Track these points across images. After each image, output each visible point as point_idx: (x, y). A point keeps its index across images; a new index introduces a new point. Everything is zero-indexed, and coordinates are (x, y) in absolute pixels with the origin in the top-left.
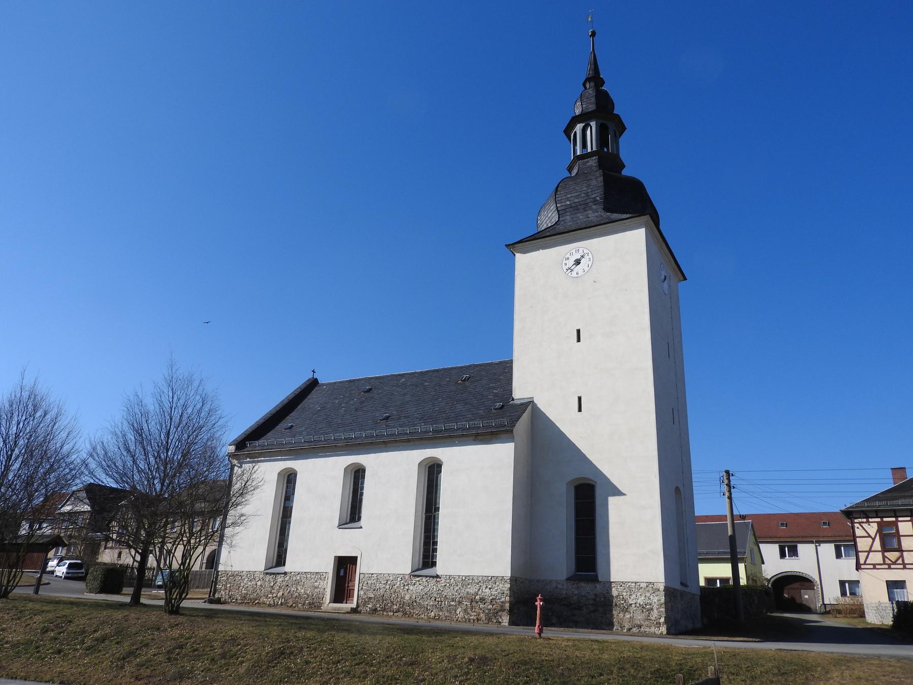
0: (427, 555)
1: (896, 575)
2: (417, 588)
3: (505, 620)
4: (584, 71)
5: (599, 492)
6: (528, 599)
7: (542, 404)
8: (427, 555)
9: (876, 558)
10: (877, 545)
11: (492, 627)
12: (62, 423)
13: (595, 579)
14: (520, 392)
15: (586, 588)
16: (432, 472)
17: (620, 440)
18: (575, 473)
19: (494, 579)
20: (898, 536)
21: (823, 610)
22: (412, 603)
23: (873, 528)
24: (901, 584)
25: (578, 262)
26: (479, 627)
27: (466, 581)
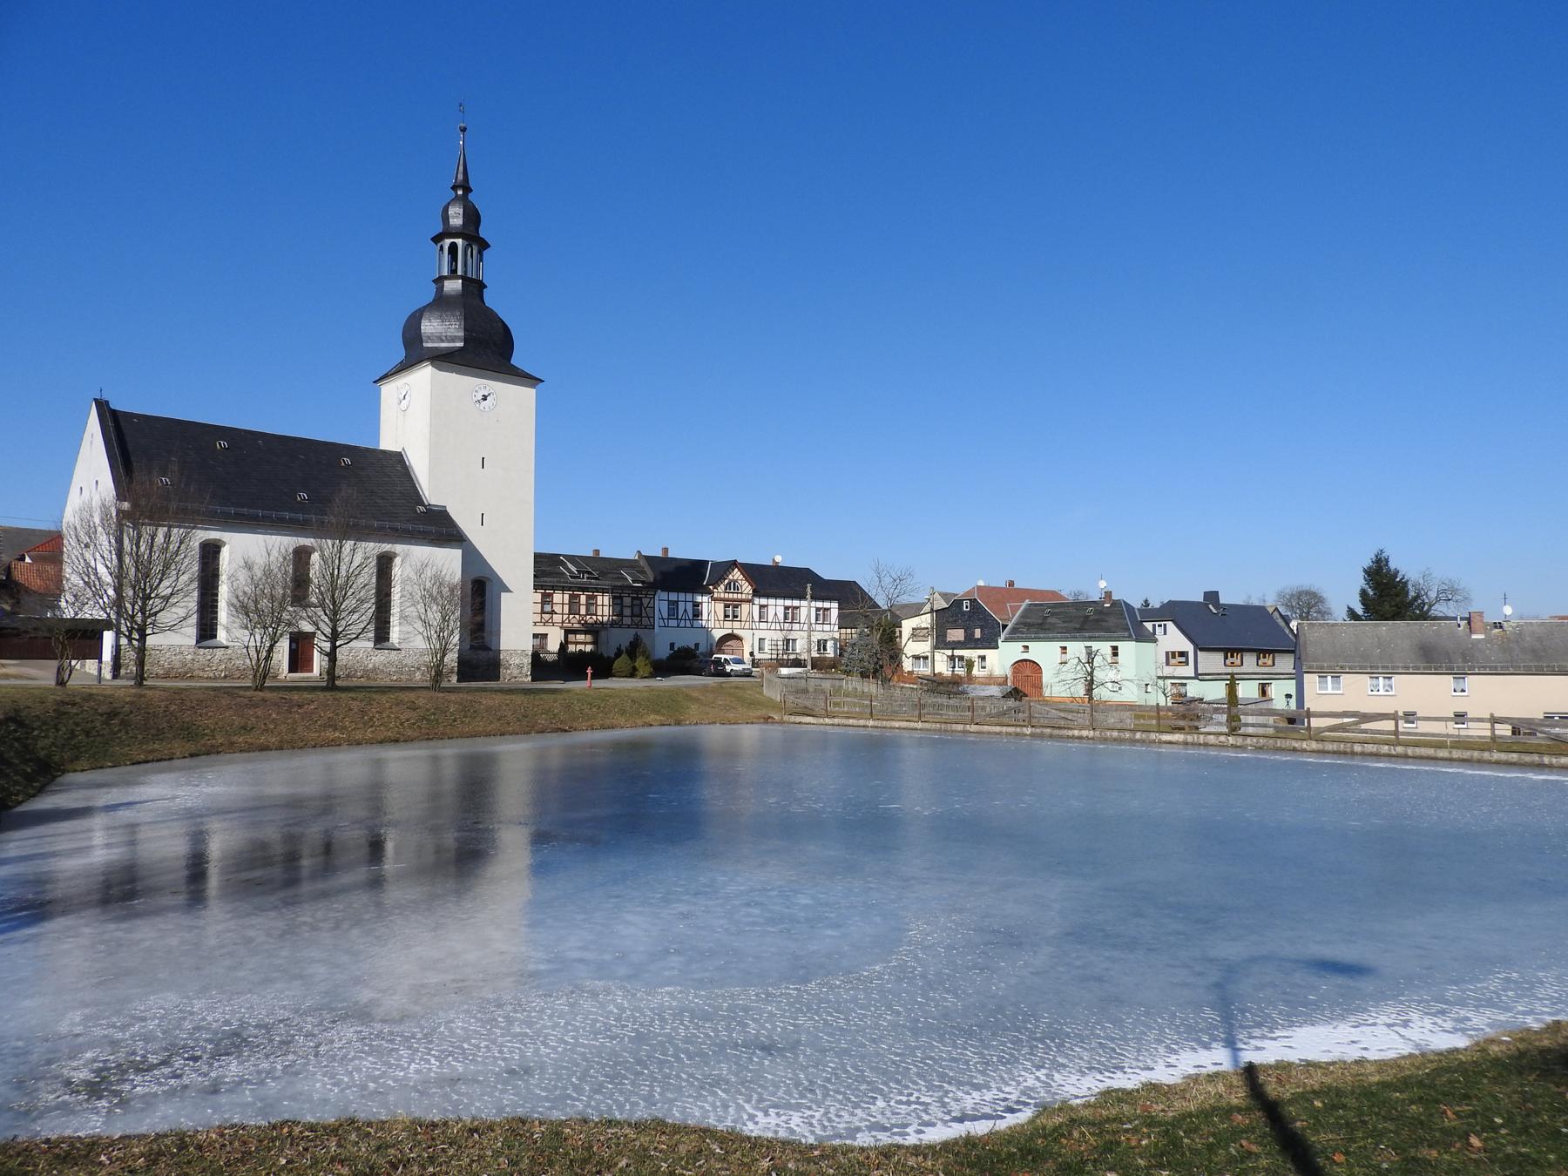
3: (454, 679)
4: (452, 176)
15: (483, 655)
22: (375, 669)
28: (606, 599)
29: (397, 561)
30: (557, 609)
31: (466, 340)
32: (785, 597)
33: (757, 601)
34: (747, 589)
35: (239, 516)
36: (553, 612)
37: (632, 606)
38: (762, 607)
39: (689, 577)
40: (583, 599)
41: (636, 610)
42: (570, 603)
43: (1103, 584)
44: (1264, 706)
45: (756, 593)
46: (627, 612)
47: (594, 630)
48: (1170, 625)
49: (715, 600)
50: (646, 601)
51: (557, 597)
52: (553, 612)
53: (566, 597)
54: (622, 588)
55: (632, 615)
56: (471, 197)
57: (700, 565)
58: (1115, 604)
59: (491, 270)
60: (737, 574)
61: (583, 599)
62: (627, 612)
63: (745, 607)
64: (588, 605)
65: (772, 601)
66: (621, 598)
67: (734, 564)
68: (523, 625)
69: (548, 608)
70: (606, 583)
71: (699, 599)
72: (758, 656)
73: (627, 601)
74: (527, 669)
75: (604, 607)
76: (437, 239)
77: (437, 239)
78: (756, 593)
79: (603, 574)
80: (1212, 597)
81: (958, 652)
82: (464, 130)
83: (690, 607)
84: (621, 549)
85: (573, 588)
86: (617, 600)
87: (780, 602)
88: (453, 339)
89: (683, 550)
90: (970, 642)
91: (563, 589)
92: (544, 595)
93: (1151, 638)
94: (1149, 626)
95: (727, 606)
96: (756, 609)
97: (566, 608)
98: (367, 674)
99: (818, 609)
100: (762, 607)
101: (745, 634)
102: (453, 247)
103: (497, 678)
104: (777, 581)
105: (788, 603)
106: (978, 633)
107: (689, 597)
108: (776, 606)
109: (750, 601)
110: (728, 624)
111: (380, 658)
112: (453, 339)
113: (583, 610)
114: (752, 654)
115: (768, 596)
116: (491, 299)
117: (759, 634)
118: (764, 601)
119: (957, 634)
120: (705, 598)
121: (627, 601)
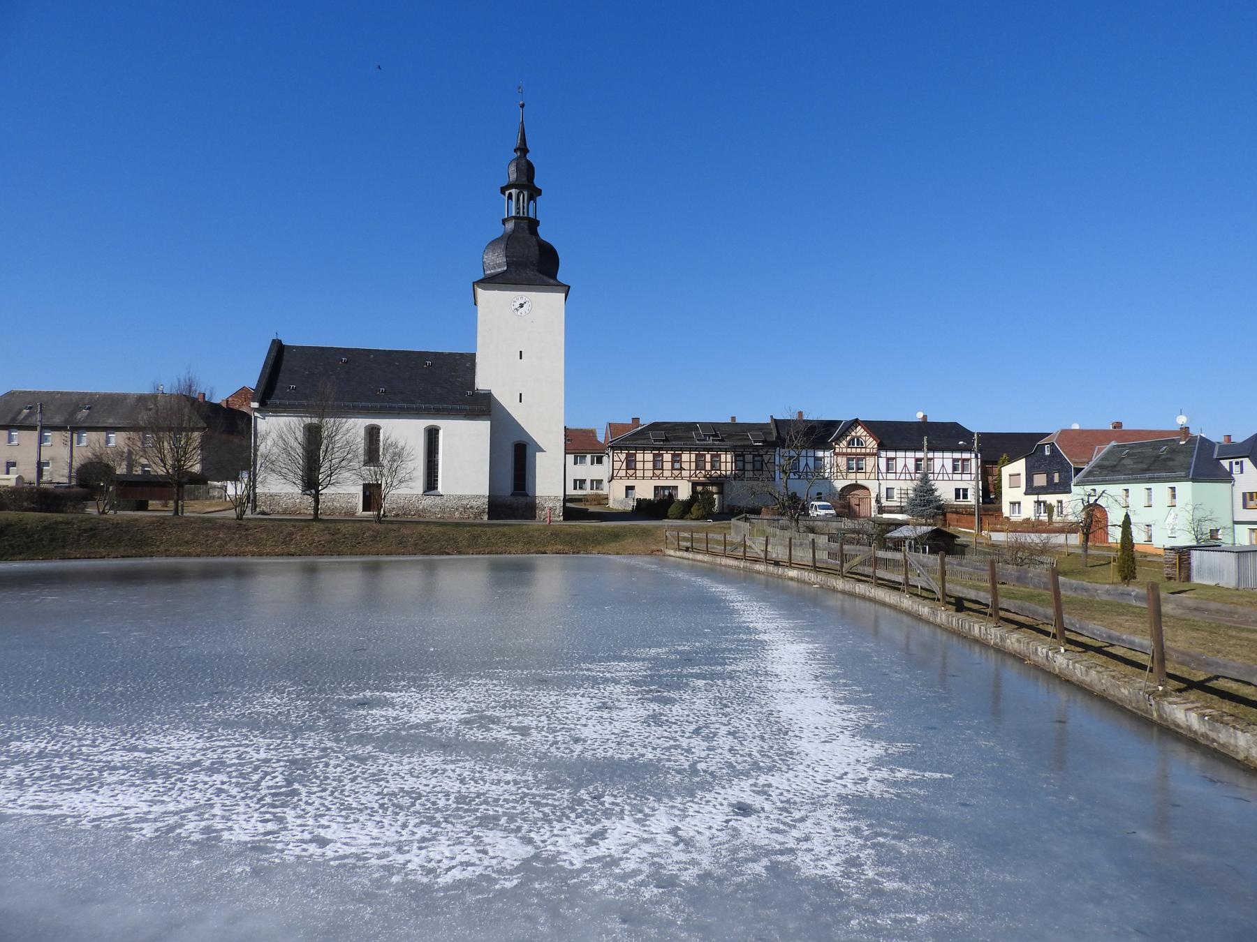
0: (431, 482)
1: (630, 483)
2: (428, 502)
3: (486, 517)
4: (517, 142)
5: (529, 451)
6: (498, 508)
7: (496, 394)
8: (431, 482)
9: (623, 473)
10: (624, 466)
11: (478, 521)
12: (407, 448)
13: (527, 495)
14: (481, 383)
15: (522, 500)
16: (432, 434)
17: (544, 423)
18: (516, 439)
19: (478, 497)
20: (635, 461)
21: (630, 505)
22: (424, 510)
23: (623, 457)
24: (632, 488)
25: (522, 306)
26: (471, 521)
27: (460, 498)
28: (729, 457)
29: (441, 433)
30: (685, 466)
31: (508, 264)
32: (953, 450)
33: (883, 454)
34: (871, 444)
35: (402, 409)
36: (681, 469)
37: (754, 462)
38: (888, 459)
39: (822, 434)
40: (708, 457)
41: (758, 465)
42: (696, 462)
43: (1182, 420)
44: (1212, 542)
45: (882, 447)
46: (749, 467)
47: (720, 482)
48: (1247, 461)
49: (837, 454)
50: (766, 458)
51: (639, 456)
52: (681, 469)
53: (693, 456)
54: (744, 447)
55: (673, 469)
56: (529, 157)
57: (832, 424)
58: (1192, 440)
59: (543, 210)
60: (860, 431)
61: (708, 457)
62: (749, 467)
63: (870, 461)
64: (712, 462)
65: (900, 454)
66: (743, 455)
67: (856, 422)
68: (552, 479)
69: (677, 465)
70: (728, 444)
71: (820, 454)
72: (884, 503)
73: (749, 458)
74: (559, 511)
75: (727, 463)
76: (503, 190)
77: (503, 190)
78: (882, 447)
79: (730, 436)
80: (1118, 425)
81: (1042, 498)
82: (522, 106)
83: (811, 462)
84: (749, 416)
85: (700, 450)
86: (739, 457)
87: (910, 454)
88: (499, 265)
89: (815, 413)
90: (1051, 488)
91: (690, 450)
92: (673, 456)
93: (1227, 477)
94: (1226, 463)
95: (848, 460)
96: (883, 462)
97: (693, 465)
98: (418, 513)
99: (955, 460)
100: (888, 459)
101: (872, 485)
102: (510, 195)
103: (534, 517)
104: (894, 436)
105: (957, 455)
106: (1056, 480)
107: (811, 453)
108: (906, 459)
109: (877, 455)
110: (852, 476)
111: (428, 502)
112: (499, 265)
113: (708, 467)
114: (878, 501)
115: (896, 450)
116: (544, 233)
117: (890, 484)
118: (891, 454)
119: (1040, 480)
120: (827, 454)
121: (749, 458)
